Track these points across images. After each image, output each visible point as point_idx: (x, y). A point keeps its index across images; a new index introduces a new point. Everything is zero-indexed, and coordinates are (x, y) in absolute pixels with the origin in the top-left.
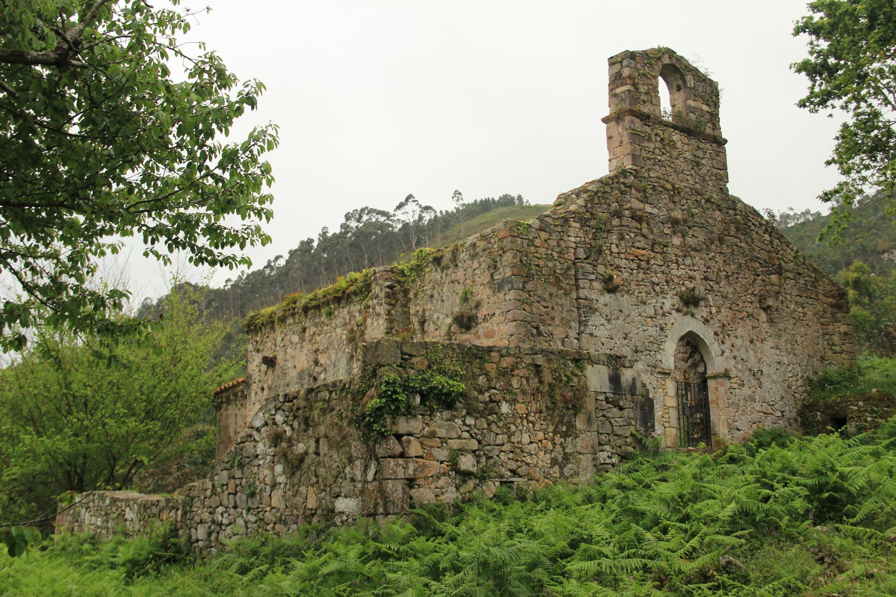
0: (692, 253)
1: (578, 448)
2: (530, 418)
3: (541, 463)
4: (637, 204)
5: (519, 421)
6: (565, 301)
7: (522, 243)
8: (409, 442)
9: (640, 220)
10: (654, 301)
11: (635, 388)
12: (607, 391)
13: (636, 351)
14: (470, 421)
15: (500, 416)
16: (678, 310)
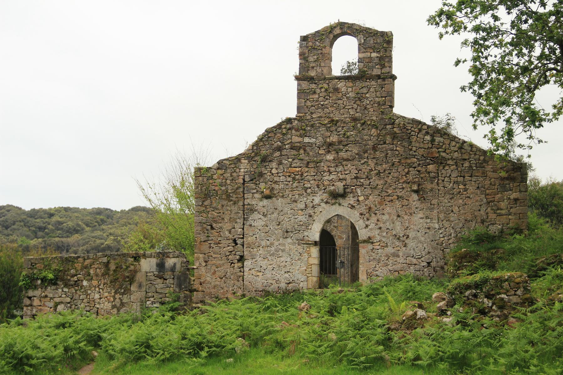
0: (344, 163)
1: (132, 300)
2: (100, 287)
3: (105, 308)
4: (296, 139)
5: (93, 288)
6: (235, 209)
7: (203, 179)
8: (33, 300)
9: (298, 149)
10: (305, 199)
11: (175, 268)
12: (155, 270)
13: (287, 232)
14: (66, 290)
15: (82, 286)
16: (327, 203)
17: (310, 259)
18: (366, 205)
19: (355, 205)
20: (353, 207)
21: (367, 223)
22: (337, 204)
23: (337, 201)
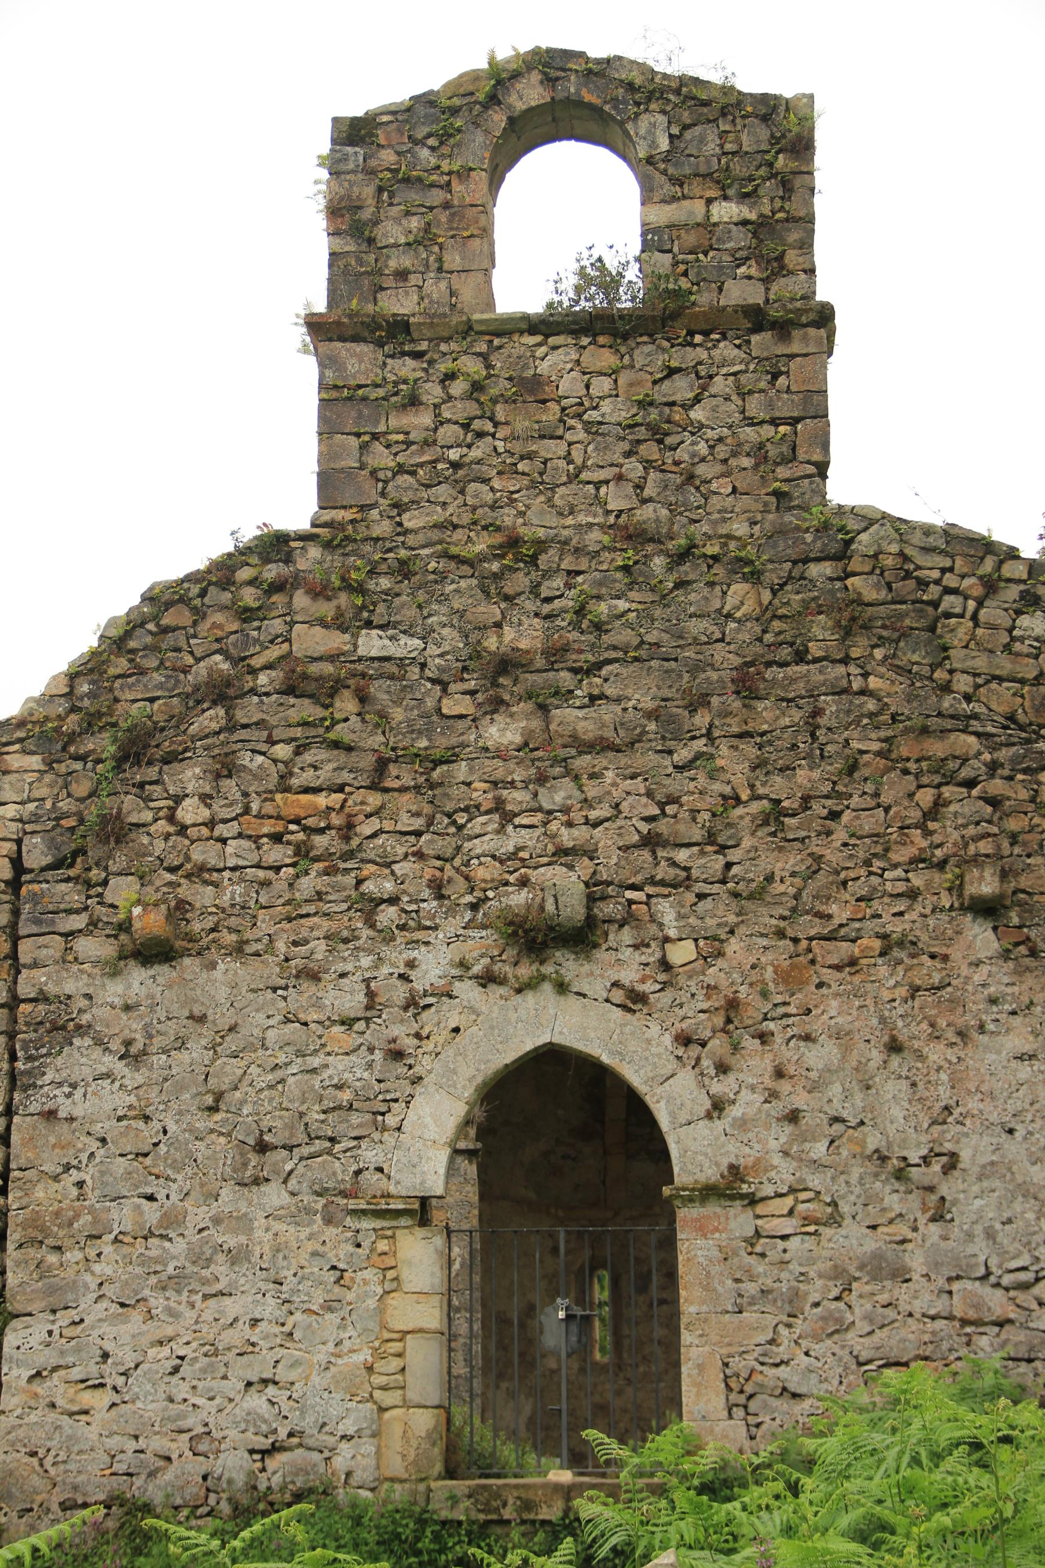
16: (488, 979)
17: (394, 1301)
18: (711, 989)
19: (648, 987)
20: (635, 1000)
21: (717, 1088)
22: (547, 987)
23: (548, 969)
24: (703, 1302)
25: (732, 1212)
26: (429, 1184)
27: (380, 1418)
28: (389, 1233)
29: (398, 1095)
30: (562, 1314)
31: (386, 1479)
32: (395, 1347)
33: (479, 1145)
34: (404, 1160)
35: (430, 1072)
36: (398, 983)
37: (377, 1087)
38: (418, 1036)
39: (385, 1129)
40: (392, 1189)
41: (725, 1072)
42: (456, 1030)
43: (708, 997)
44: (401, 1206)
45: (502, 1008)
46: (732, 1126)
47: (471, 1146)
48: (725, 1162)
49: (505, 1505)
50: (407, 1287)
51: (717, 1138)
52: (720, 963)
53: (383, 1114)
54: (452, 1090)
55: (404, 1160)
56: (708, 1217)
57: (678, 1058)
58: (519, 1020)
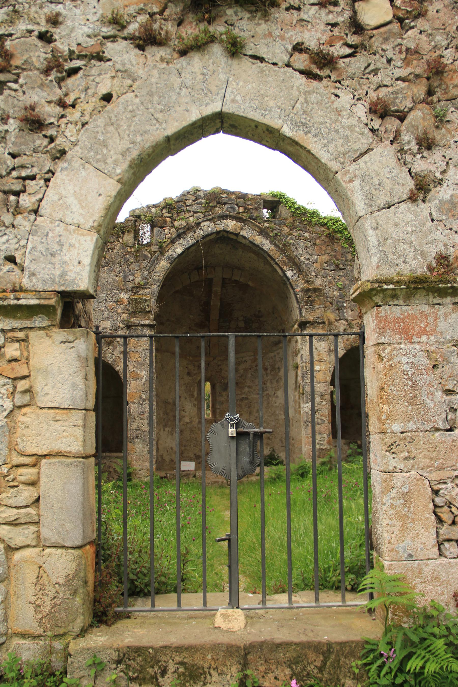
16: (147, 40)
17: (25, 418)
18: (411, 53)
19: (339, 50)
20: (321, 65)
21: (420, 165)
22: (217, 49)
23: (218, 28)
24: (409, 419)
25: (442, 310)
26: (71, 276)
27: (8, 559)
28: (21, 335)
29: (35, 170)
30: (232, 432)
31: (17, 634)
32: (27, 474)
33: (155, 323)
34: (40, 247)
35: (75, 144)
36: (40, 44)
37: (10, 162)
38: (62, 104)
39: (18, 210)
40: (26, 282)
41: (429, 148)
42: (107, 98)
43: (407, 62)
44: (34, 302)
45: (162, 72)
46: (439, 209)
47: (151, 323)
48: (432, 252)
49: (164, 672)
50: (42, 401)
51: (422, 224)
52: (421, 23)
53: (17, 194)
54: (101, 166)
55: (40, 247)
56: (414, 317)
57: (373, 130)
58: (183, 86)
